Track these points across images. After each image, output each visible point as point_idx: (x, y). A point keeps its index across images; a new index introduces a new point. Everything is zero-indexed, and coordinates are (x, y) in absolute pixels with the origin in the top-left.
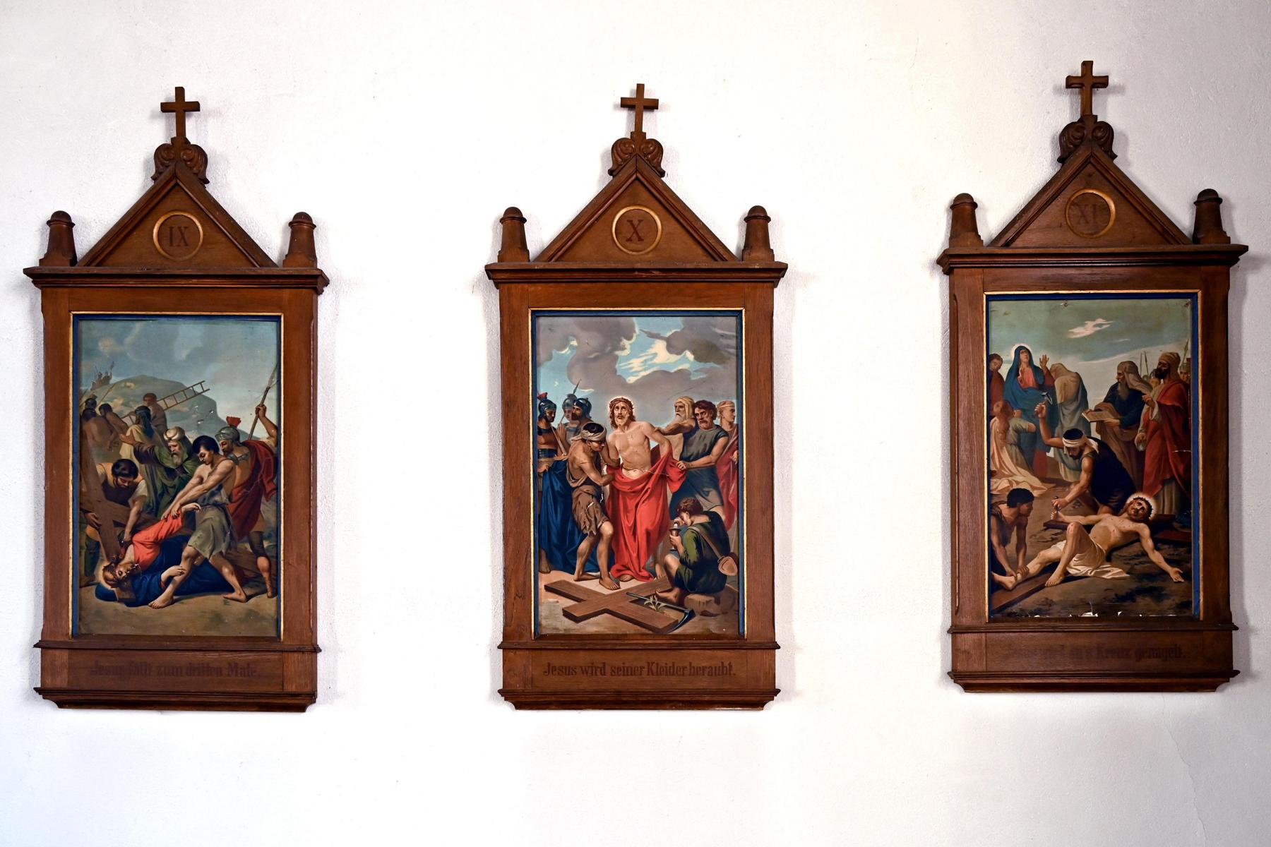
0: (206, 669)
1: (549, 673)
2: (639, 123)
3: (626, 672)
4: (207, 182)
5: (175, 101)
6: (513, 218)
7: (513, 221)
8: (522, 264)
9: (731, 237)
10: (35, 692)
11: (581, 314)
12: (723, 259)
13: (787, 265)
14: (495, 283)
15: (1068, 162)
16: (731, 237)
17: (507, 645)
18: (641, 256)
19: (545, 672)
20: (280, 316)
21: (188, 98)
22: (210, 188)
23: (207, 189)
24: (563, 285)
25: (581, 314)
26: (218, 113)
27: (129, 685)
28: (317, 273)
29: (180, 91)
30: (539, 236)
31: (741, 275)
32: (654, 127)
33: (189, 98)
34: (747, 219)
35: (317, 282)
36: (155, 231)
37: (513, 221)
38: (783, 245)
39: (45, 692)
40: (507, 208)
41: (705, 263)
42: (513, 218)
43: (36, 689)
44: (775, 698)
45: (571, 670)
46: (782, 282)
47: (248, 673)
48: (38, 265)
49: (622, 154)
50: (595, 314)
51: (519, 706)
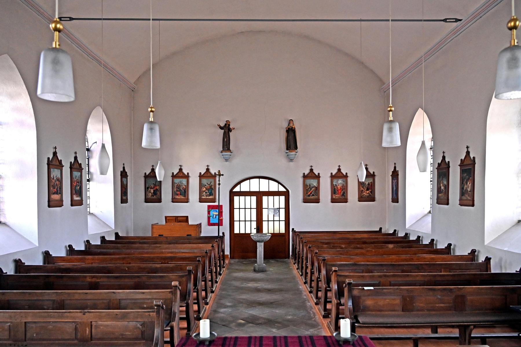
30: (175, 174)
39: (199, 202)
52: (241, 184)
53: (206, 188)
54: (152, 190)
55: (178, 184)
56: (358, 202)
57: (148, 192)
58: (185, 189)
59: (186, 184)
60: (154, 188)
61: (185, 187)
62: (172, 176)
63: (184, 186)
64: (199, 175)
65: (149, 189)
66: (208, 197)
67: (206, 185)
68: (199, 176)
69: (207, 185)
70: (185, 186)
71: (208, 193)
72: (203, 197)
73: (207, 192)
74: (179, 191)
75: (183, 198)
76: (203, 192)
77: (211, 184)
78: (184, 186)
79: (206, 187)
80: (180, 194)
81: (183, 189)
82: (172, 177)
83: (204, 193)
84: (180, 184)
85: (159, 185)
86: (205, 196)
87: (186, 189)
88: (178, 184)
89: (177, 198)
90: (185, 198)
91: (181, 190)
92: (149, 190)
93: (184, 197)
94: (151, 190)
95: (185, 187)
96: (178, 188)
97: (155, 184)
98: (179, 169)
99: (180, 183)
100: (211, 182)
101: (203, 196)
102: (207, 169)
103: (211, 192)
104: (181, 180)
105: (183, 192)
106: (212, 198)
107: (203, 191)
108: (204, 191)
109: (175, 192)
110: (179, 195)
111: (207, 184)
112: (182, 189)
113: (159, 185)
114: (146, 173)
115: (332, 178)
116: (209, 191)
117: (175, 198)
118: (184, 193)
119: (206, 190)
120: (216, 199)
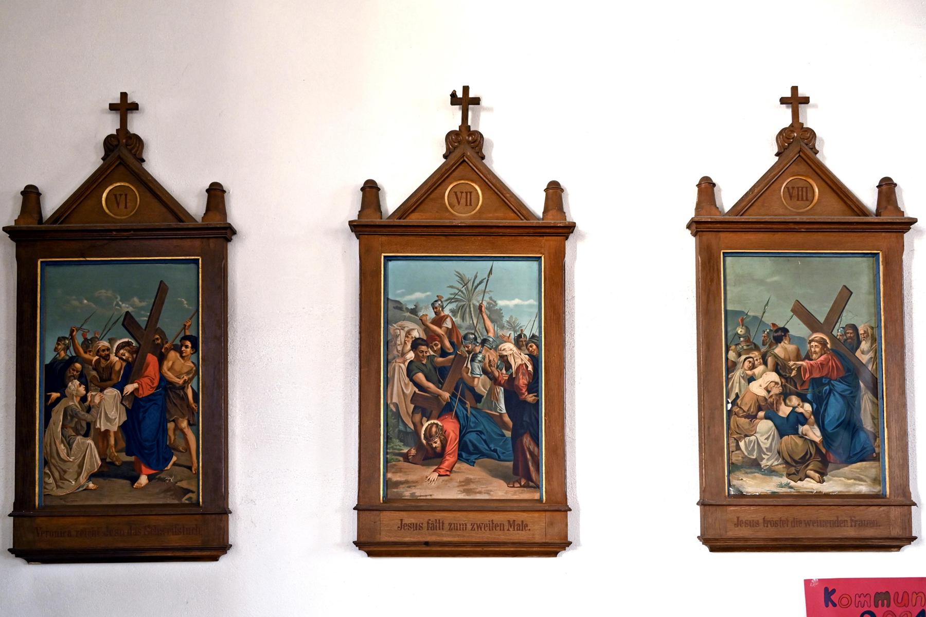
0: (493, 526)
1: (401, 528)
2: (124, 122)
3: (502, 528)
4: (143, 161)
5: (799, 96)
6: (371, 187)
7: (707, 188)
8: (377, 221)
9: (869, 198)
10: (8, 552)
11: (474, 259)
12: (181, 221)
13: (575, 223)
14: (356, 235)
15: (784, 155)
16: (536, 203)
17: (17, 513)
18: (462, 216)
19: (399, 527)
20: (541, 257)
21: (472, 95)
22: (145, 166)
23: (143, 166)
24: (780, 233)
25: (474, 259)
26: (815, 106)
27: (869, 532)
28: (227, 226)
29: (795, 89)
30: (392, 202)
31: (220, 231)
32: (137, 125)
33: (788, 94)
34: (362, 189)
35: (227, 233)
36: (105, 195)
37: (707, 188)
38: (574, 211)
39: (359, 544)
40: (552, 180)
41: (174, 224)
42: (371, 187)
43: (9, 550)
44: (912, 543)
45: (412, 527)
46: (571, 236)
47: (463, 528)
48: (357, 219)
49: (453, 143)
50: (93, 263)
51: (713, 549)
52: (782, 326)
53: (780, 368)
54: (111, 393)
55: (439, 321)
56: (361, 557)
57: (58, 416)
58: (523, 381)
59: (530, 326)
60: (131, 372)
61: (518, 358)
62: (355, 227)
63: (509, 348)
64: (690, 213)
65: (75, 386)
66: (810, 485)
67: (780, 334)
68: (355, 227)
69: (797, 328)
70: (519, 342)
71: (815, 434)
72: (752, 485)
73: (798, 419)
74: (446, 409)
75: (500, 490)
76: (752, 417)
77: (847, 318)
78: (509, 348)
79: (779, 350)
80: (467, 452)
81: (495, 381)
82: (354, 244)
83: (765, 426)
84: (464, 325)
85: (194, 341)
86: (771, 472)
87: (533, 387)
88: (439, 321)
89: (420, 492)
90: (526, 495)
91: (478, 398)
92: (75, 403)
93: (509, 480)
94: (95, 397)
95: (518, 358)
96: (440, 374)
97: (142, 320)
98: (451, 137)
99: (461, 310)
100: (846, 294)
101: (754, 465)
102: (110, 144)
103: (851, 425)
104: (473, 269)
105: (498, 421)
106: (863, 488)
107: (747, 404)
108: (767, 408)
109: (394, 415)
110: (450, 459)
111: (800, 311)
112: (481, 384)
113: (194, 341)
114: (226, 184)
115: (377, 241)
116: (820, 404)
117: (392, 504)
118: (516, 436)
119: (785, 395)
120: (225, 512)
